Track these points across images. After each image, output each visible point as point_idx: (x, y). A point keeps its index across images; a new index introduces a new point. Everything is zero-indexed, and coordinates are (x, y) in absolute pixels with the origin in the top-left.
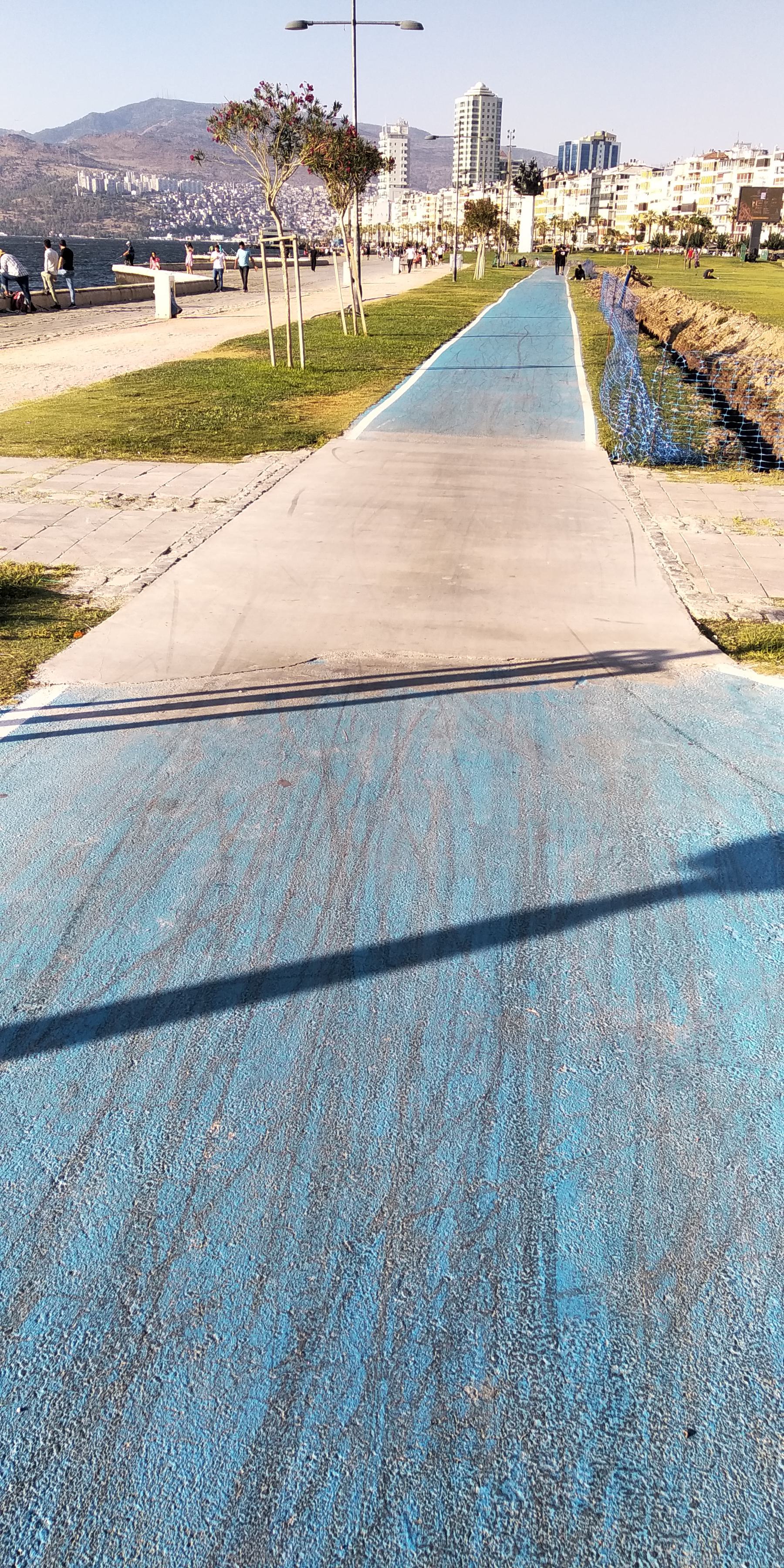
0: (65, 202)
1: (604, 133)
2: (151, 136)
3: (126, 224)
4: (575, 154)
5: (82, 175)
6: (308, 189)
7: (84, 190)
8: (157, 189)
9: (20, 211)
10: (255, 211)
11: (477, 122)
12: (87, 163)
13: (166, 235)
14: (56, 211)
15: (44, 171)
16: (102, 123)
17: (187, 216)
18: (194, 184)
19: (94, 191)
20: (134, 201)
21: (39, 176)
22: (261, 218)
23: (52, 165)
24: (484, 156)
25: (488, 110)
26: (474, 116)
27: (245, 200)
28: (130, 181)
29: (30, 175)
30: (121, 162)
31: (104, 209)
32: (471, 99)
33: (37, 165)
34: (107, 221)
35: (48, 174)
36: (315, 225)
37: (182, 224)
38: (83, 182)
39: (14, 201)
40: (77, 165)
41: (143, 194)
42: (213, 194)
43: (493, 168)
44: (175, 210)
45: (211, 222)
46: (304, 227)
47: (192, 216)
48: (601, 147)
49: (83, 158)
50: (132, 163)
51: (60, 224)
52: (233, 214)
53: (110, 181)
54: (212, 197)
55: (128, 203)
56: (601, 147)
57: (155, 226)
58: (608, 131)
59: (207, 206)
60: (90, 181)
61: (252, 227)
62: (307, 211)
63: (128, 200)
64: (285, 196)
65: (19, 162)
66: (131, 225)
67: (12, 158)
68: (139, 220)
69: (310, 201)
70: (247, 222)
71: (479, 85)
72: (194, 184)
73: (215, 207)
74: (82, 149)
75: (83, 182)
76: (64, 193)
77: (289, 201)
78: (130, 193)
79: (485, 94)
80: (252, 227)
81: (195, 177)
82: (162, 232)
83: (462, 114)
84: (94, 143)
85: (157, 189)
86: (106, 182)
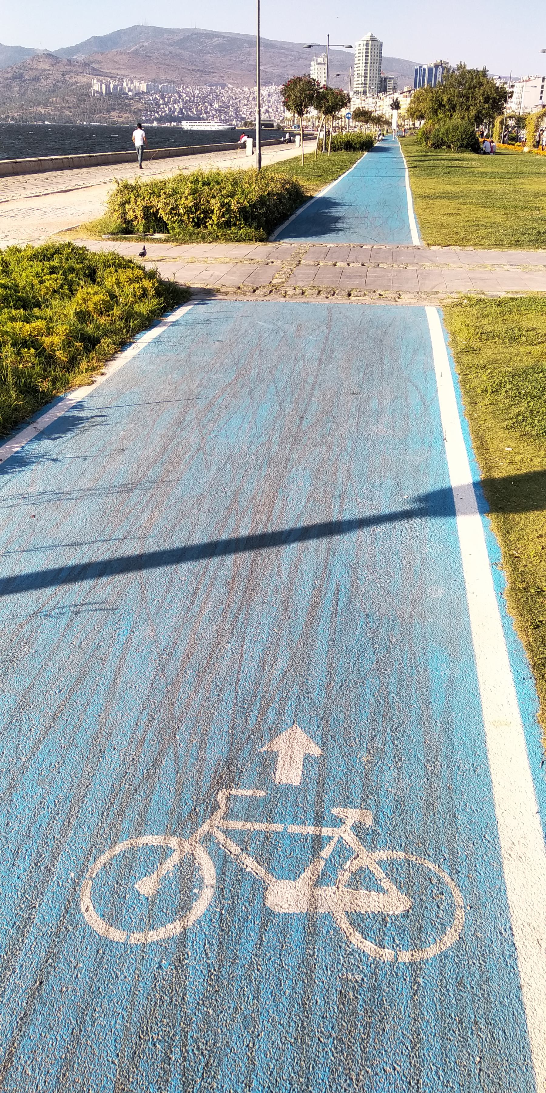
0: (85, 100)
1: (441, 61)
2: (136, 53)
3: (126, 115)
4: (424, 73)
5: (95, 81)
6: (246, 89)
7: (97, 92)
8: (145, 91)
9: (55, 107)
10: (211, 105)
11: (368, 53)
12: (96, 73)
13: (152, 122)
14: (79, 107)
15: (68, 79)
16: (102, 43)
17: (166, 109)
18: (170, 87)
19: (104, 92)
20: (131, 99)
21: (65, 82)
22: (216, 110)
23: (72, 74)
24: (372, 72)
25: (375, 47)
26: (366, 52)
27: (205, 97)
28: (127, 85)
29: (58, 82)
30: (119, 72)
31: (111, 105)
32: (365, 43)
33: (63, 75)
34: (113, 113)
35: (70, 81)
36: (252, 114)
37: (163, 114)
38: (96, 86)
39: (50, 100)
40: (90, 74)
41: (136, 94)
42: (183, 94)
43: (377, 79)
44: (158, 105)
45: (182, 113)
46: (244, 116)
47: (170, 108)
48: (440, 69)
49: (94, 69)
50: (126, 72)
51: (82, 116)
52: (197, 108)
53: (114, 85)
54: (182, 96)
55: (126, 101)
56: (440, 69)
57: (145, 116)
58: (444, 60)
59: (179, 102)
60: (101, 85)
61: (209, 116)
62: (246, 105)
63: (127, 99)
64: (231, 95)
65: (50, 72)
66: (129, 116)
67: (46, 70)
68: (134, 112)
69: (248, 98)
70: (206, 113)
71: (369, 34)
72: (170, 87)
73: (185, 103)
74: (92, 62)
75: (96, 86)
76: (84, 94)
77: (234, 98)
78: (127, 94)
79: (373, 39)
80: (209, 116)
81: (169, 82)
82: (150, 120)
83: (359, 51)
84: (99, 58)
85: (145, 91)
86: (112, 86)
